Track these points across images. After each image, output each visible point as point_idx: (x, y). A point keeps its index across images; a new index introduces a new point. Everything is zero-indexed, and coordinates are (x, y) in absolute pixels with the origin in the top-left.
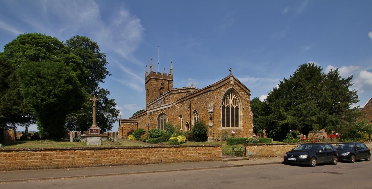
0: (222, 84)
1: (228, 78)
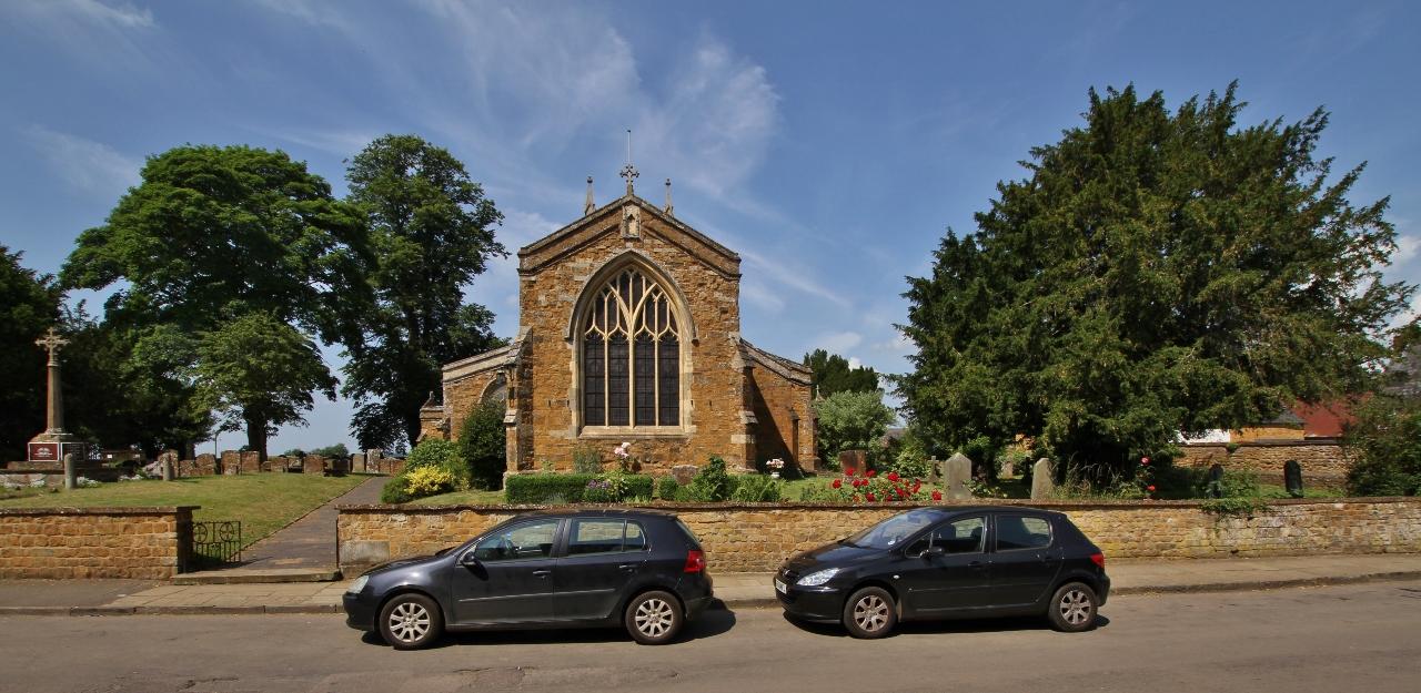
0: (577, 239)
1: (611, 213)
